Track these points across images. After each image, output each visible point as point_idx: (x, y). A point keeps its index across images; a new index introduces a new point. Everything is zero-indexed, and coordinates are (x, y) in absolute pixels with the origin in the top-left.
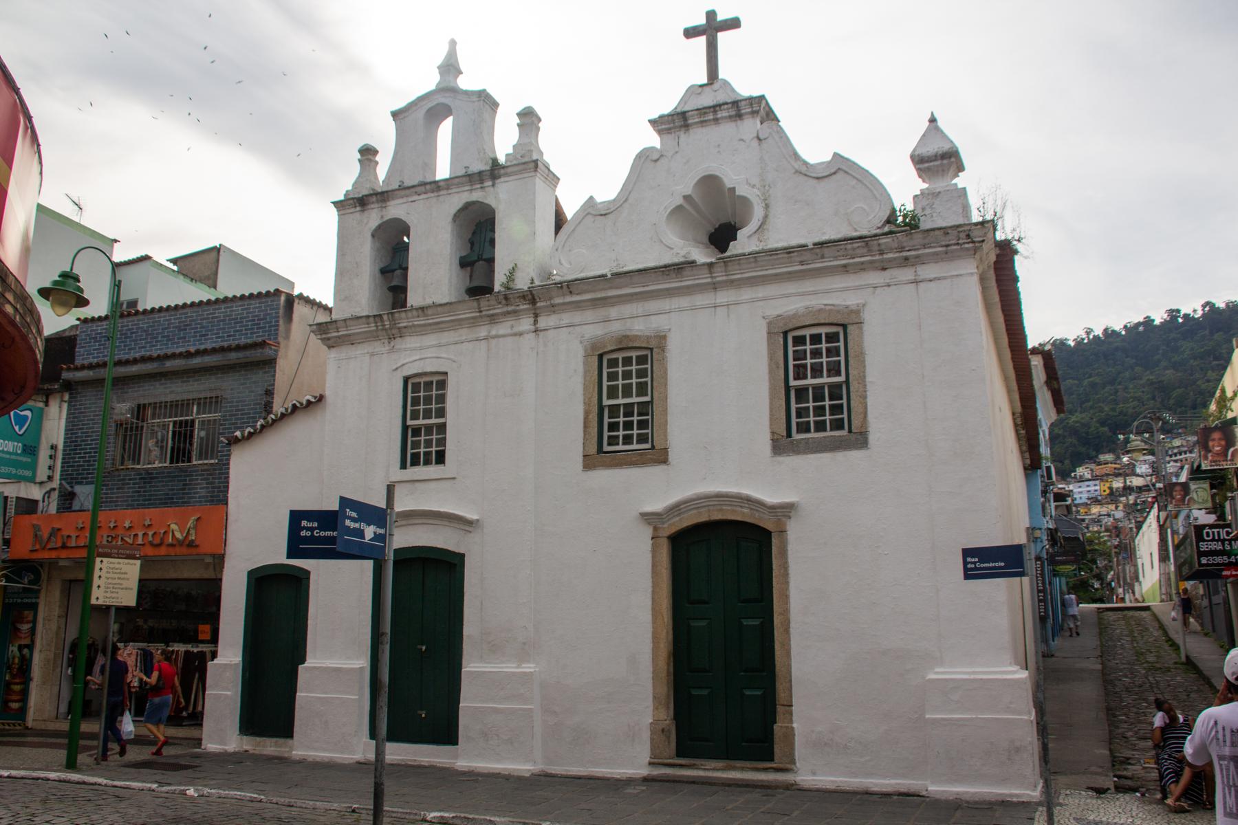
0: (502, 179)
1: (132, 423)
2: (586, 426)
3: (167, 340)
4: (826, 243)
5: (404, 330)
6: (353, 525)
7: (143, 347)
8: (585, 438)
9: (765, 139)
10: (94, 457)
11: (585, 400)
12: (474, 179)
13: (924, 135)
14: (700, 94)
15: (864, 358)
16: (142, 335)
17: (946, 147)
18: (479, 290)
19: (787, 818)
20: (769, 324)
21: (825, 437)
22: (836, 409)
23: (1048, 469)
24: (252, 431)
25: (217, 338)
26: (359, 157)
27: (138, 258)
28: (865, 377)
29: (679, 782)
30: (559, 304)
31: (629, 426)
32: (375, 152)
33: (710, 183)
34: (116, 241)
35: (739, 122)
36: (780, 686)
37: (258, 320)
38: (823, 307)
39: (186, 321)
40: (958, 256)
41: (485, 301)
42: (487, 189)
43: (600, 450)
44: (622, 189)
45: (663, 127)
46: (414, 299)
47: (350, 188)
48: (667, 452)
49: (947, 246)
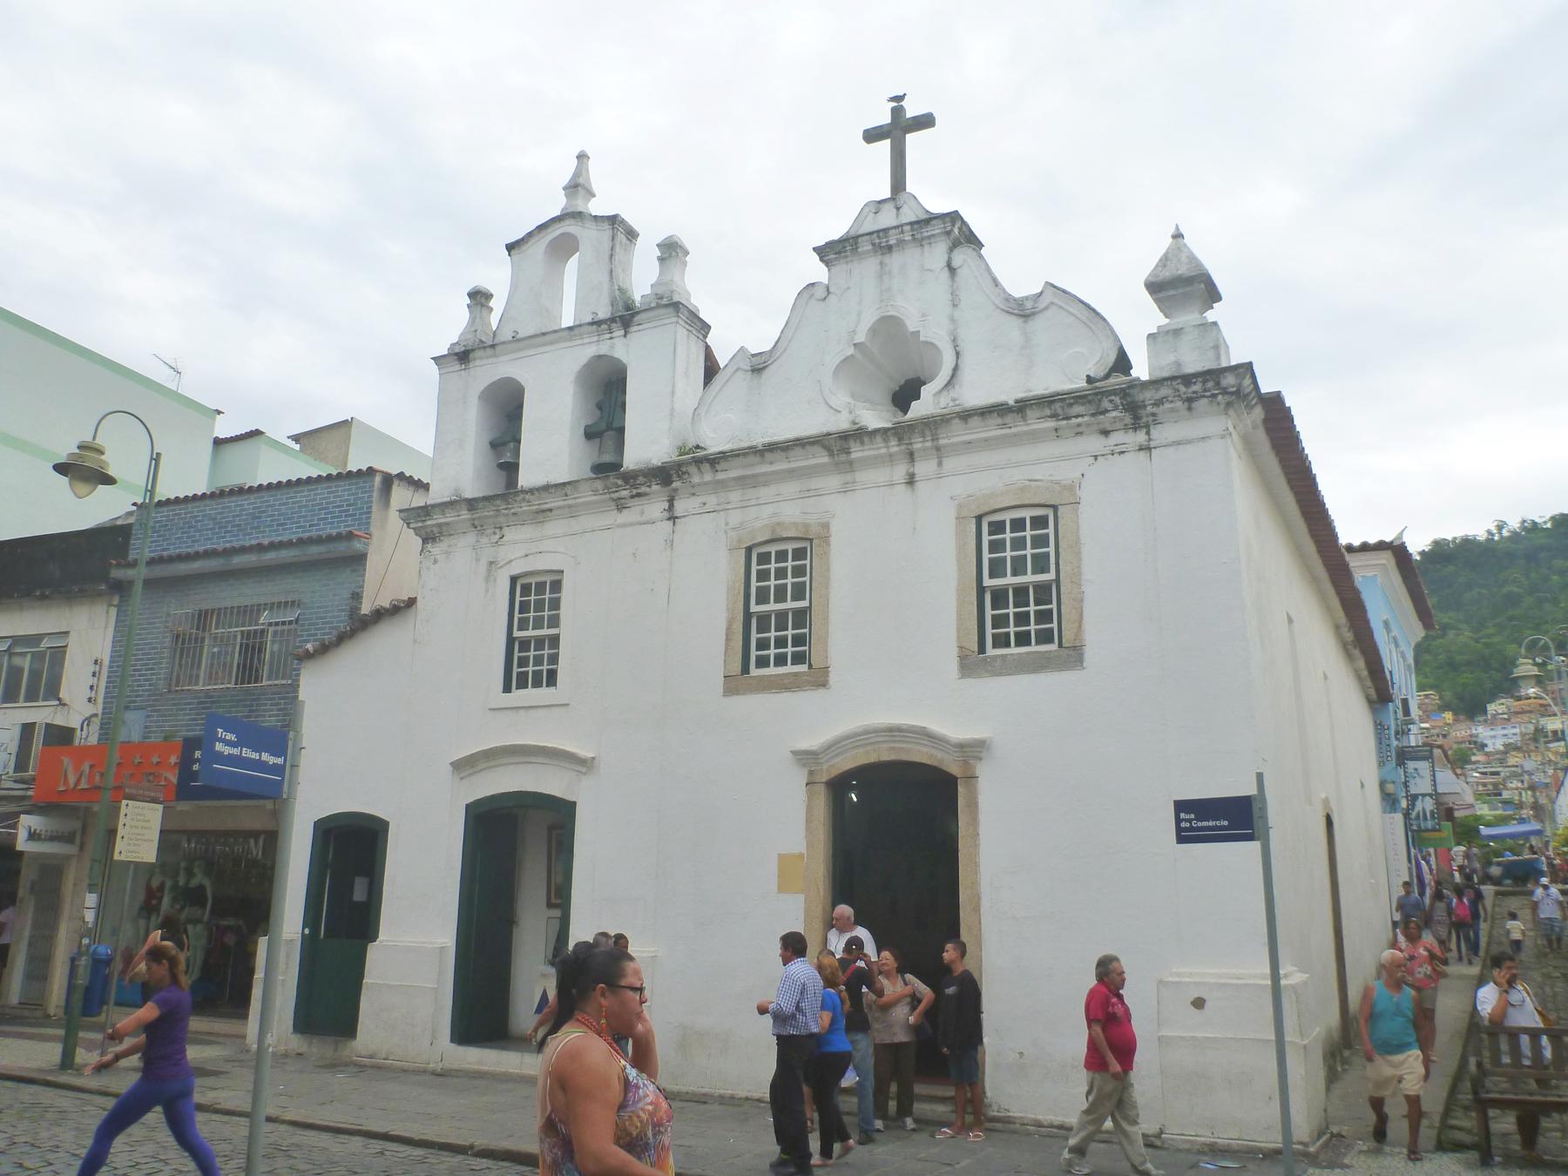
0: (478, 363)
1: (191, 634)
3: (238, 530)
6: (227, 750)
10: (134, 670)
16: (209, 524)
18: (606, 468)
20: (960, 506)
21: (1028, 653)
22: (1044, 616)
23: (1405, 702)
28: (1080, 573)
31: (781, 642)
32: (489, 296)
33: (889, 328)
34: (219, 412)
43: (745, 669)
48: (828, 672)
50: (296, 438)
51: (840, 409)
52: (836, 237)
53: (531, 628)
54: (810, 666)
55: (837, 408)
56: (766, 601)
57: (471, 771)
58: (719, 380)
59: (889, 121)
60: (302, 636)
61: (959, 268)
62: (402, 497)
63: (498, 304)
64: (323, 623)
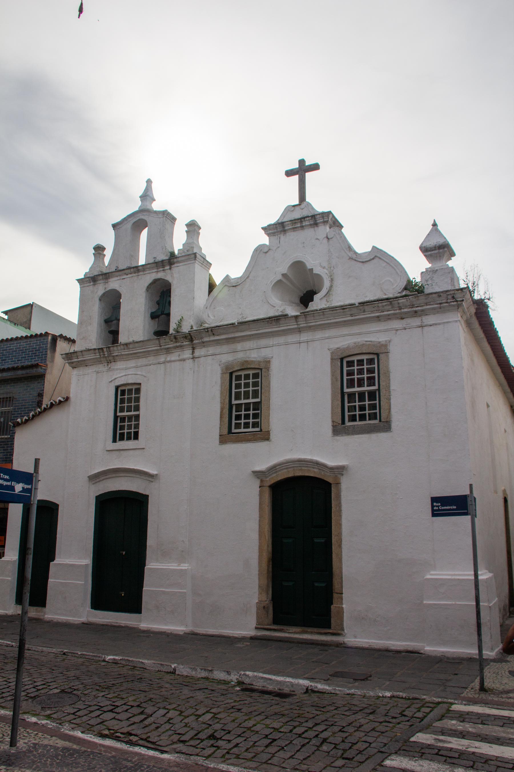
0: (176, 265)
2: (221, 417)
4: (366, 303)
11: (221, 400)
12: (159, 265)
13: (428, 234)
15: (389, 374)
17: (441, 241)
20: (332, 353)
21: (365, 424)
25: (11, 361)
26: (94, 252)
28: (389, 387)
29: (272, 640)
31: (247, 417)
32: (103, 249)
35: (316, 228)
38: (365, 342)
40: (448, 310)
41: (164, 340)
43: (230, 432)
44: (245, 271)
46: (123, 338)
47: (88, 271)
49: (440, 304)
50: (6, 313)
51: (275, 305)
52: (273, 222)
53: (242, 399)
55: (273, 305)
56: (240, 399)
57: (98, 480)
58: (215, 291)
60: (15, 414)
61: (331, 238)
62: (62, 347)
63: (108, 254)
64: (24, 408)
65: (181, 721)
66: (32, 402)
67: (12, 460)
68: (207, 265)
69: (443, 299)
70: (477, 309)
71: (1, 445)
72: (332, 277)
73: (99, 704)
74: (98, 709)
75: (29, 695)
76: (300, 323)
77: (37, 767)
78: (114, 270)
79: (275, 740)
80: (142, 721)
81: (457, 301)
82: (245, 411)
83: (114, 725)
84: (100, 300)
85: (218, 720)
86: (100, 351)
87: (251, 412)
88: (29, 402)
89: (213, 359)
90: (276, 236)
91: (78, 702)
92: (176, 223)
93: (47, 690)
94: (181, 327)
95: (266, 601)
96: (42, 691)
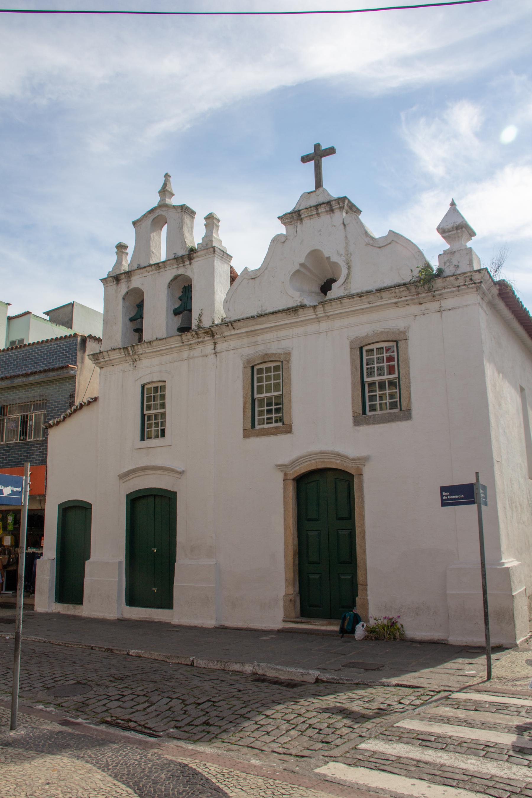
0: (195, 260)
2: (244, 411)
4: (383, 289)
5: (141, 356)
7: (3, 372)
8: (244, 419)
9: (348, 224)
11: (243, 395)
12: (179, 260)
13: (446, 215)
14: (309, 198)
15: (409, 362)
16: (3, 365)
17: (459, 221)
19: (344, 656)
20: (351, 342)
24: (58, 420)
25: (43, 364)
26: (116, 250)
27: (18, 315)
28: (409, 374)
29: (296, 632)
30: (227, 336)
31: (269, 411)
32: (126, 247)
34: (9, 304)
35: (332, 214)
36: (360, 573)
37: (66, 352)
38: (383, 330)
39: (26, 355)
40: (467, 293)
41: (186, 336)
42: (186, 267)
43: (253, 426)
44: (264, 262)
45: (287, 221)
46: (147, 336)
47: (111, 270)
49: (459, 287)
50: (47, 313)
54: (283, 424)
55: (292, 296)
57: (128, 479)
59: (313, 151)
61: (348, 224)
62: (91, 347)
63: (130, 251)
64: (58, 410)
65: (181, 709)
66: (65, 403)
67: (46, 462)
68: (227, 258)
69: (461, 281)
70: (500, 290)
71: (1, 450)
72: (349, 265)
73: (108, 694)
74: (106, 698)
75: (46, 686)
76: (319, 313)
77: (30, 747)
78: (136, 268)
79: (262, 726)
80: (145, 709)
81: (475, 283)
82: (267, 406)
83: (118, 713)
84: (124, 299)
85: (216, 708)
86: (125, 350)
87: (273, 407)
88: (62, 404)
89: (235, 354)
90: (293, 226)
91: (90, 693)
92: (196, 217)
93: (63, 681)
94: (202, 322)
95: (292, 594)
96: (59, 683)
